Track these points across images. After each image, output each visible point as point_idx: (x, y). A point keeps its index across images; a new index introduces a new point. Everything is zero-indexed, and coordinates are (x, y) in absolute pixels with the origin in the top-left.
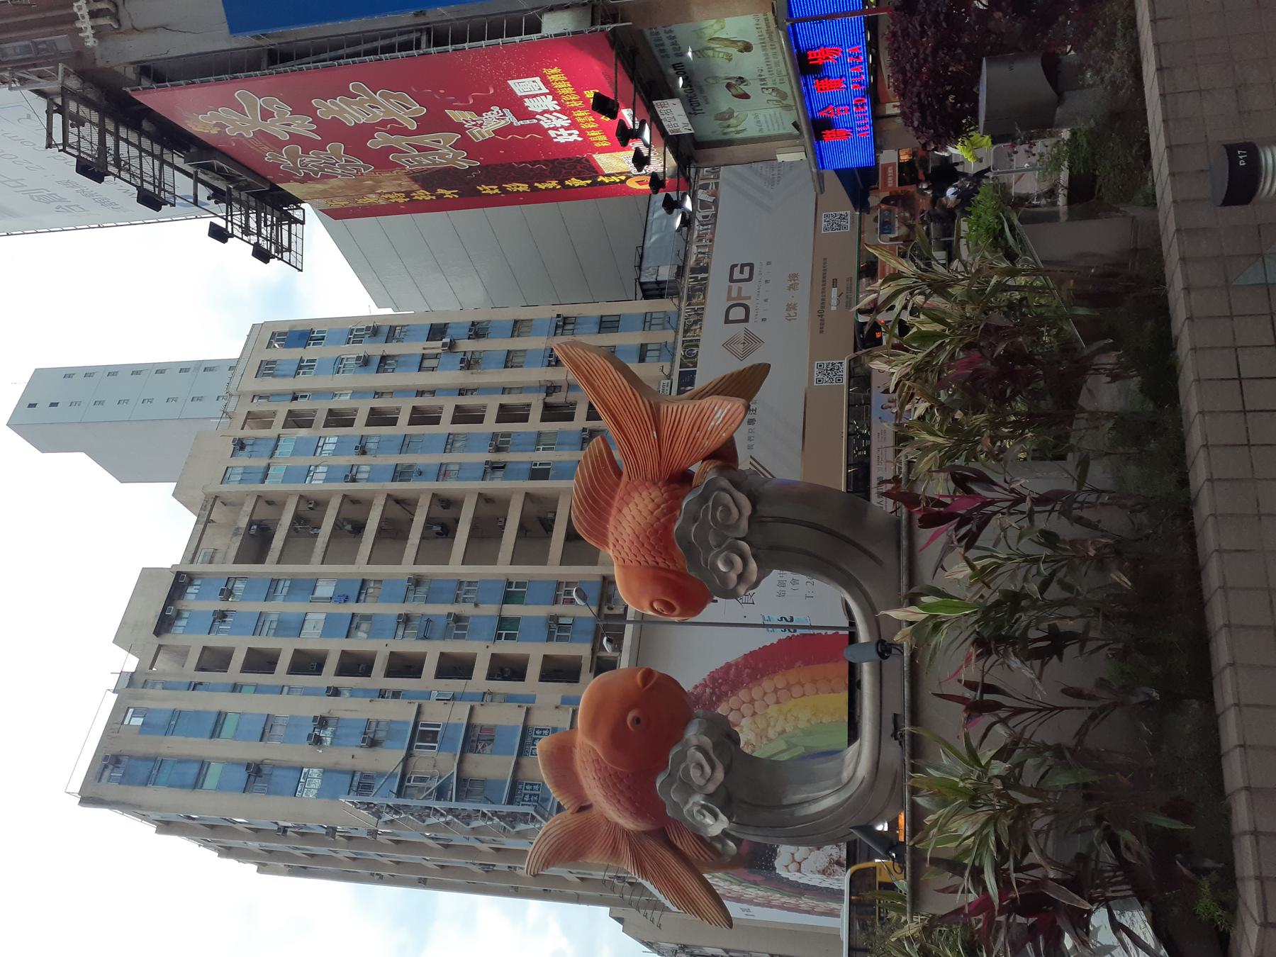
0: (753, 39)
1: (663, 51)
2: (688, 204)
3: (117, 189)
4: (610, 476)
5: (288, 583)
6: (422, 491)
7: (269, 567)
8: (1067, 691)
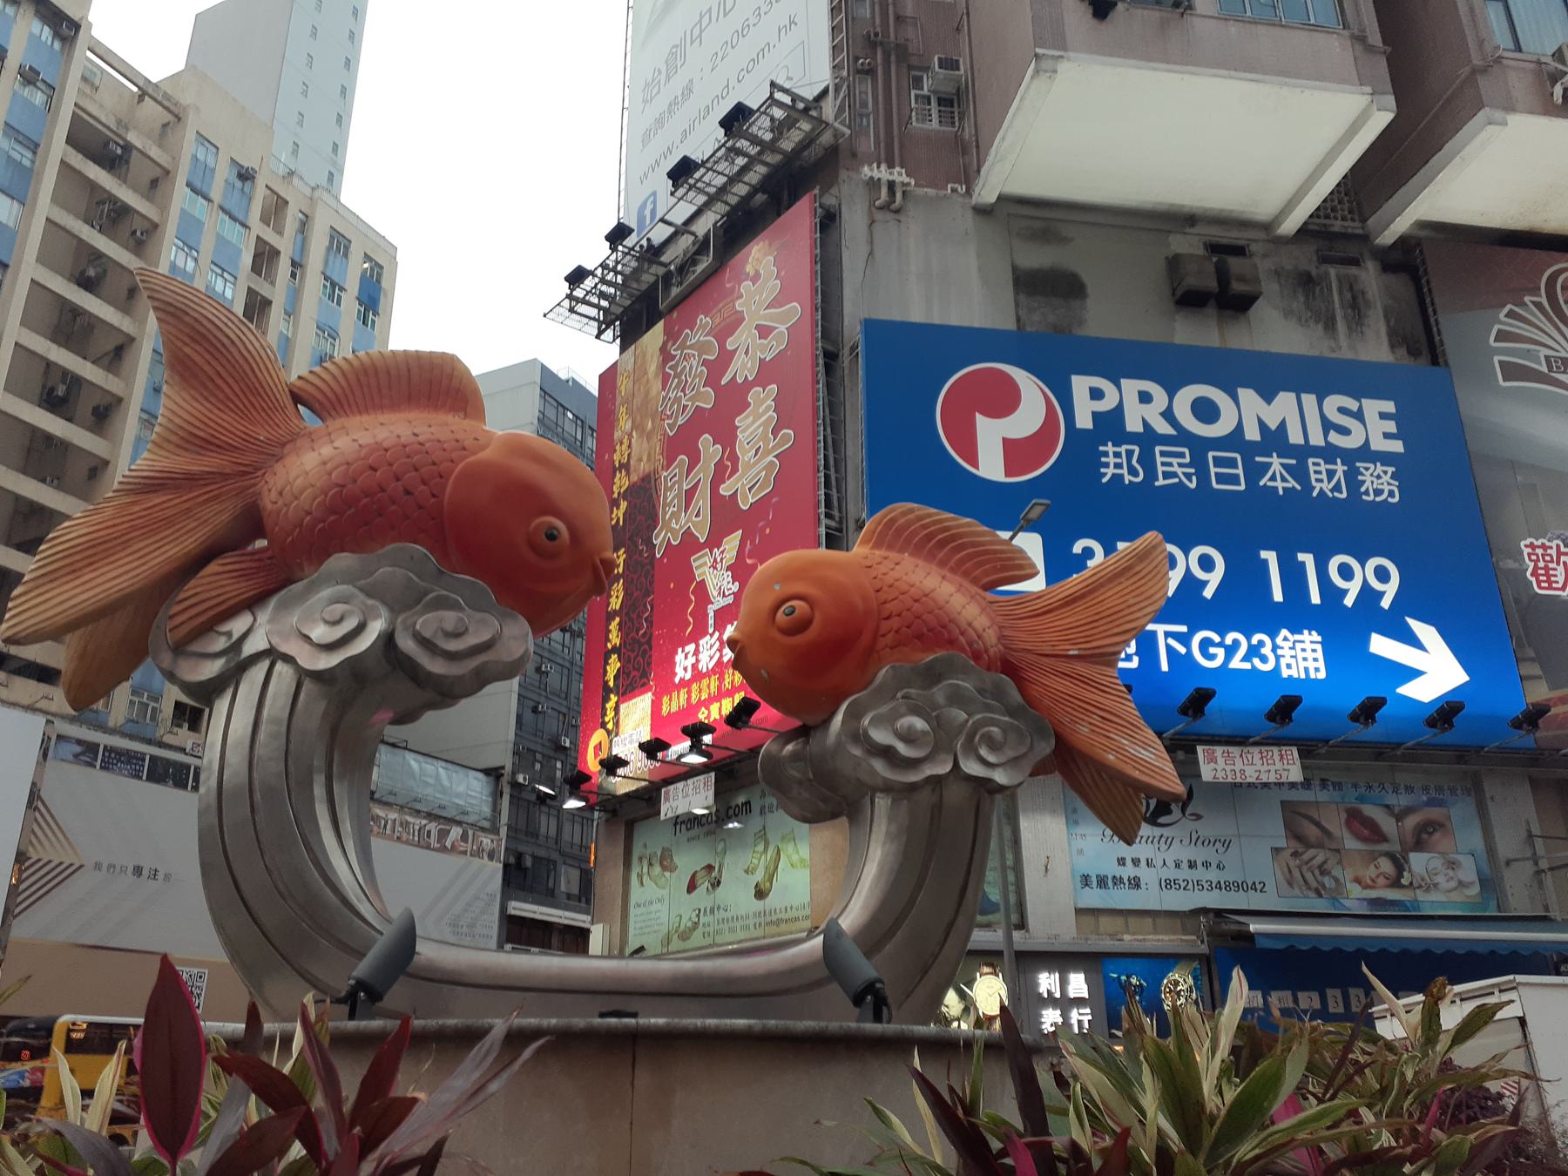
0: (772, 901)
2: (573, 804)
3: (705, 140)
4: (987, 573)
5: (26, 163)
6: (130, 384)
7: (58, 148)
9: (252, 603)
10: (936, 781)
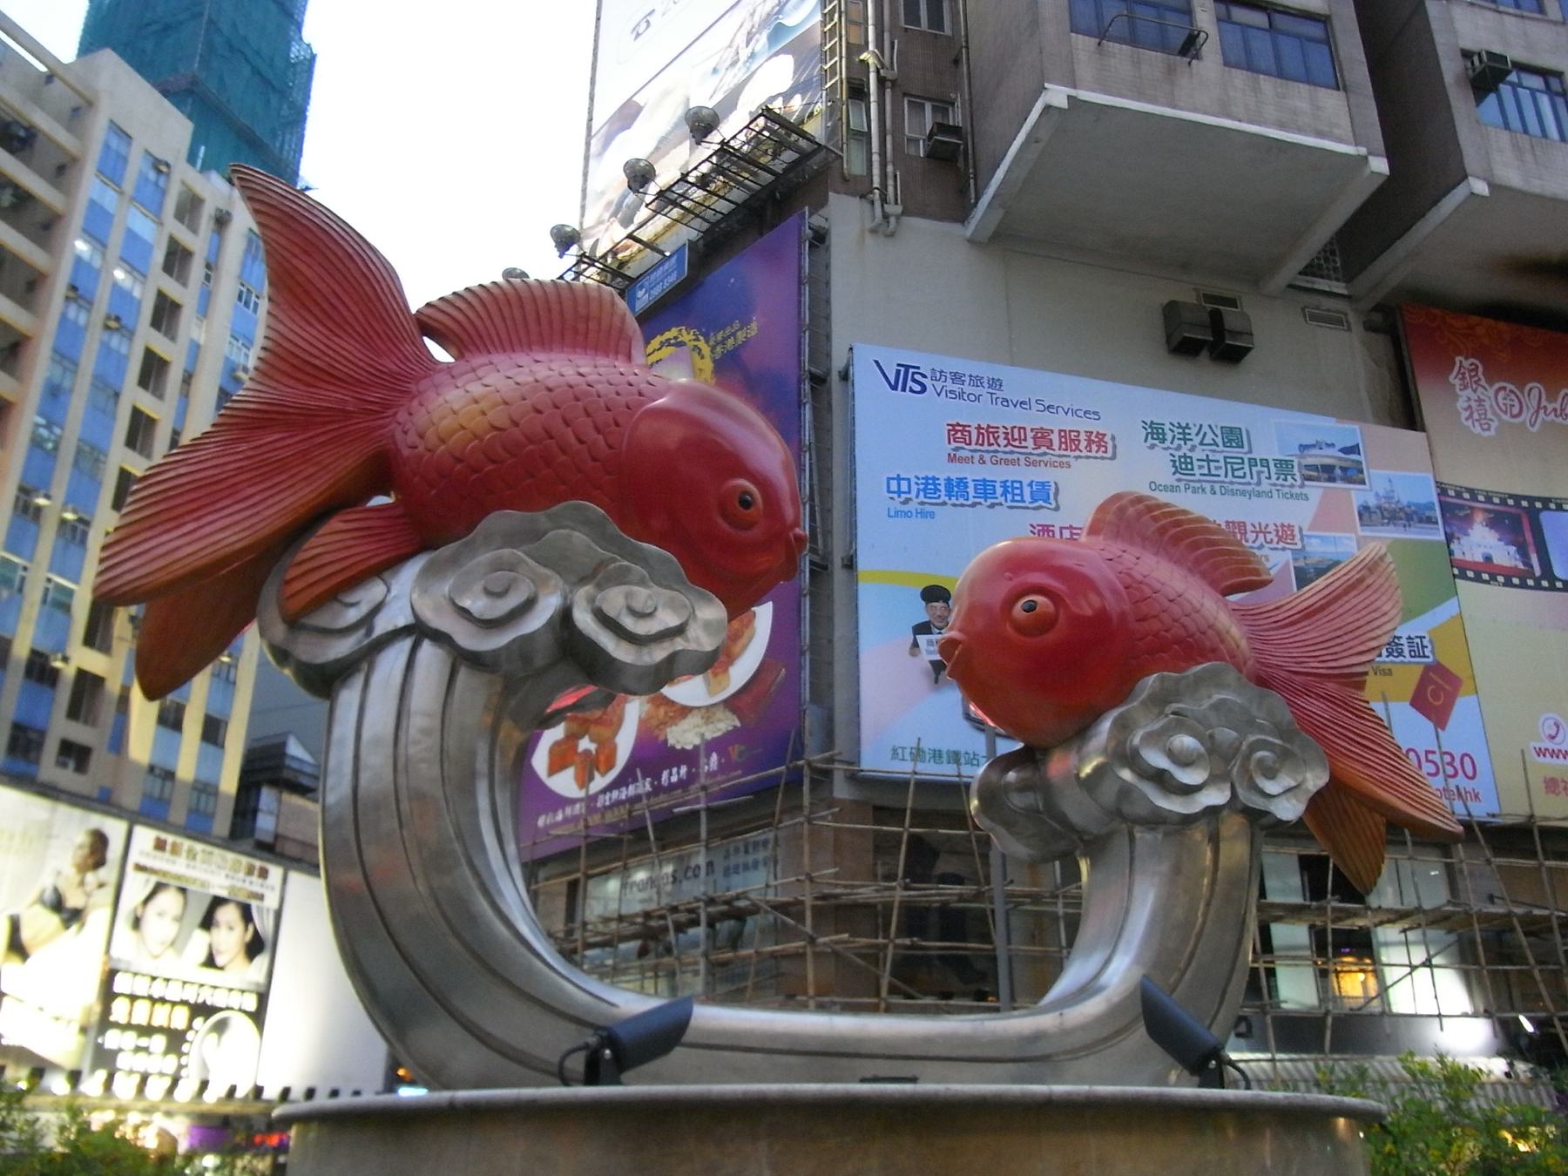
1: (737, 850)
8: (1390, 673)
9: (384, 568)
10: (1212, 812)
